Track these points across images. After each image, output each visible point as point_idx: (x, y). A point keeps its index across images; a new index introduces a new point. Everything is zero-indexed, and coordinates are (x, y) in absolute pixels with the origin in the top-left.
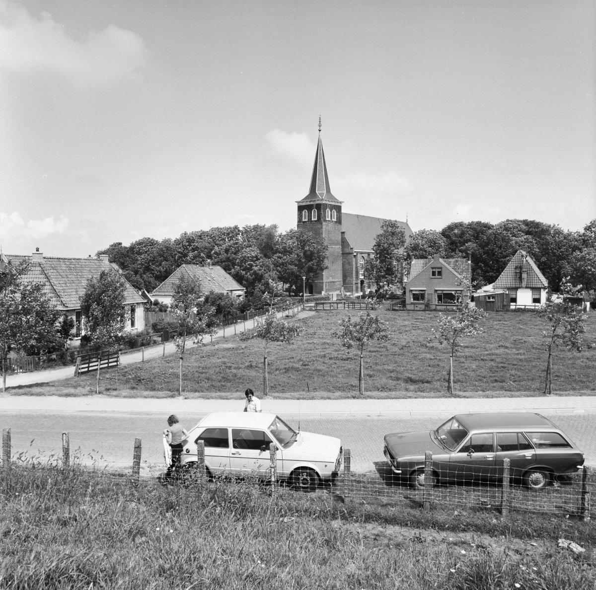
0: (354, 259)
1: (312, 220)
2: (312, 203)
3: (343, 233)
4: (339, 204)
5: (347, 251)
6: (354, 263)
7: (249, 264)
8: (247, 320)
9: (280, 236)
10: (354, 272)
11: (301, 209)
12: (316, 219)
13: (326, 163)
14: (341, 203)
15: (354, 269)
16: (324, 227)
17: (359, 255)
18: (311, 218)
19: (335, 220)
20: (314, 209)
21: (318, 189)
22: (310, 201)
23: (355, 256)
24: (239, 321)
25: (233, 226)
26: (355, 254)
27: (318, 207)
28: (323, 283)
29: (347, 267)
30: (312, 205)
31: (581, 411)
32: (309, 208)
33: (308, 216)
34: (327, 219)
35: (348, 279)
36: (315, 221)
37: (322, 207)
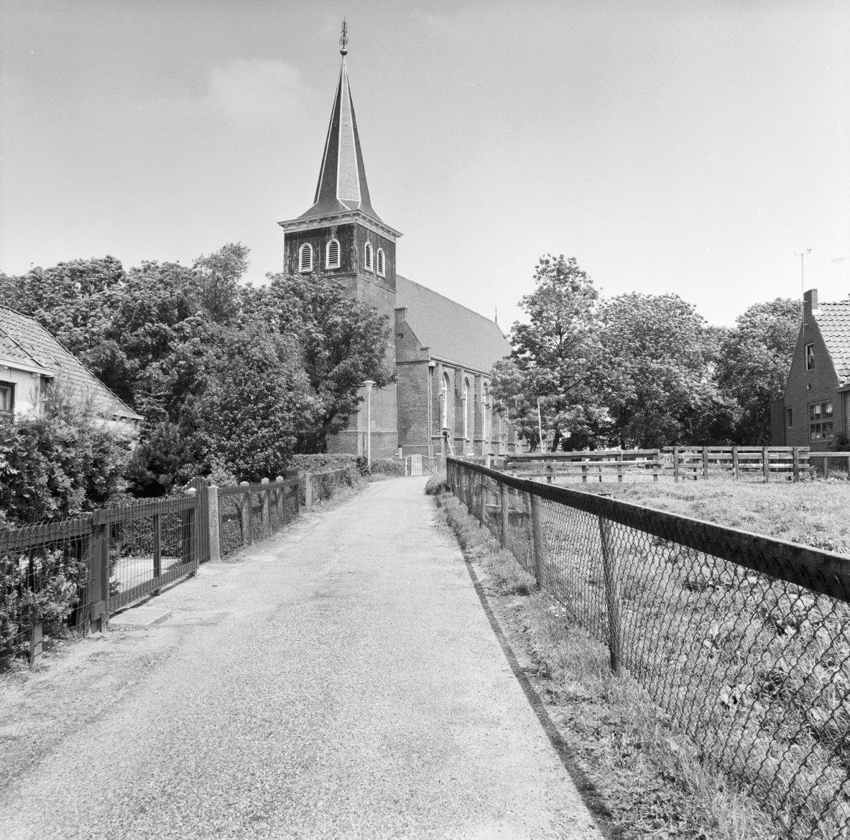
0: (429, 378)
1: (328, 267)
2: (326, 224)
3: (400, 311)
4: (391, 238)
5: (411, 355)
6: (429, 388)
7: (153, 334)
8: (206, 559)
9: (245, 293)
10: (430, 411)
11: (292, 240)
12: (338, 265)
13: (359, 136)
14: (394, 235)
15: (430, 403)
16: (360, 285)
17: (441, 370)
18: (323, 264)
19: (384, 275)
20: (333, 236)
21: (341, 192)
22: (321, 220)
23: (431, 368)
24: (131, 571)
25: (104, 257)
26: (433, 364)
27: (345, 232)
28: (356, 434)
29: (411, 397)
30: (326, 232)
31: (211, 533)
32: (318, 236)
33: (316, 259)
34: (366, 268)
35: (414, 428)
36: (335, 270)
37: (355, 232)
